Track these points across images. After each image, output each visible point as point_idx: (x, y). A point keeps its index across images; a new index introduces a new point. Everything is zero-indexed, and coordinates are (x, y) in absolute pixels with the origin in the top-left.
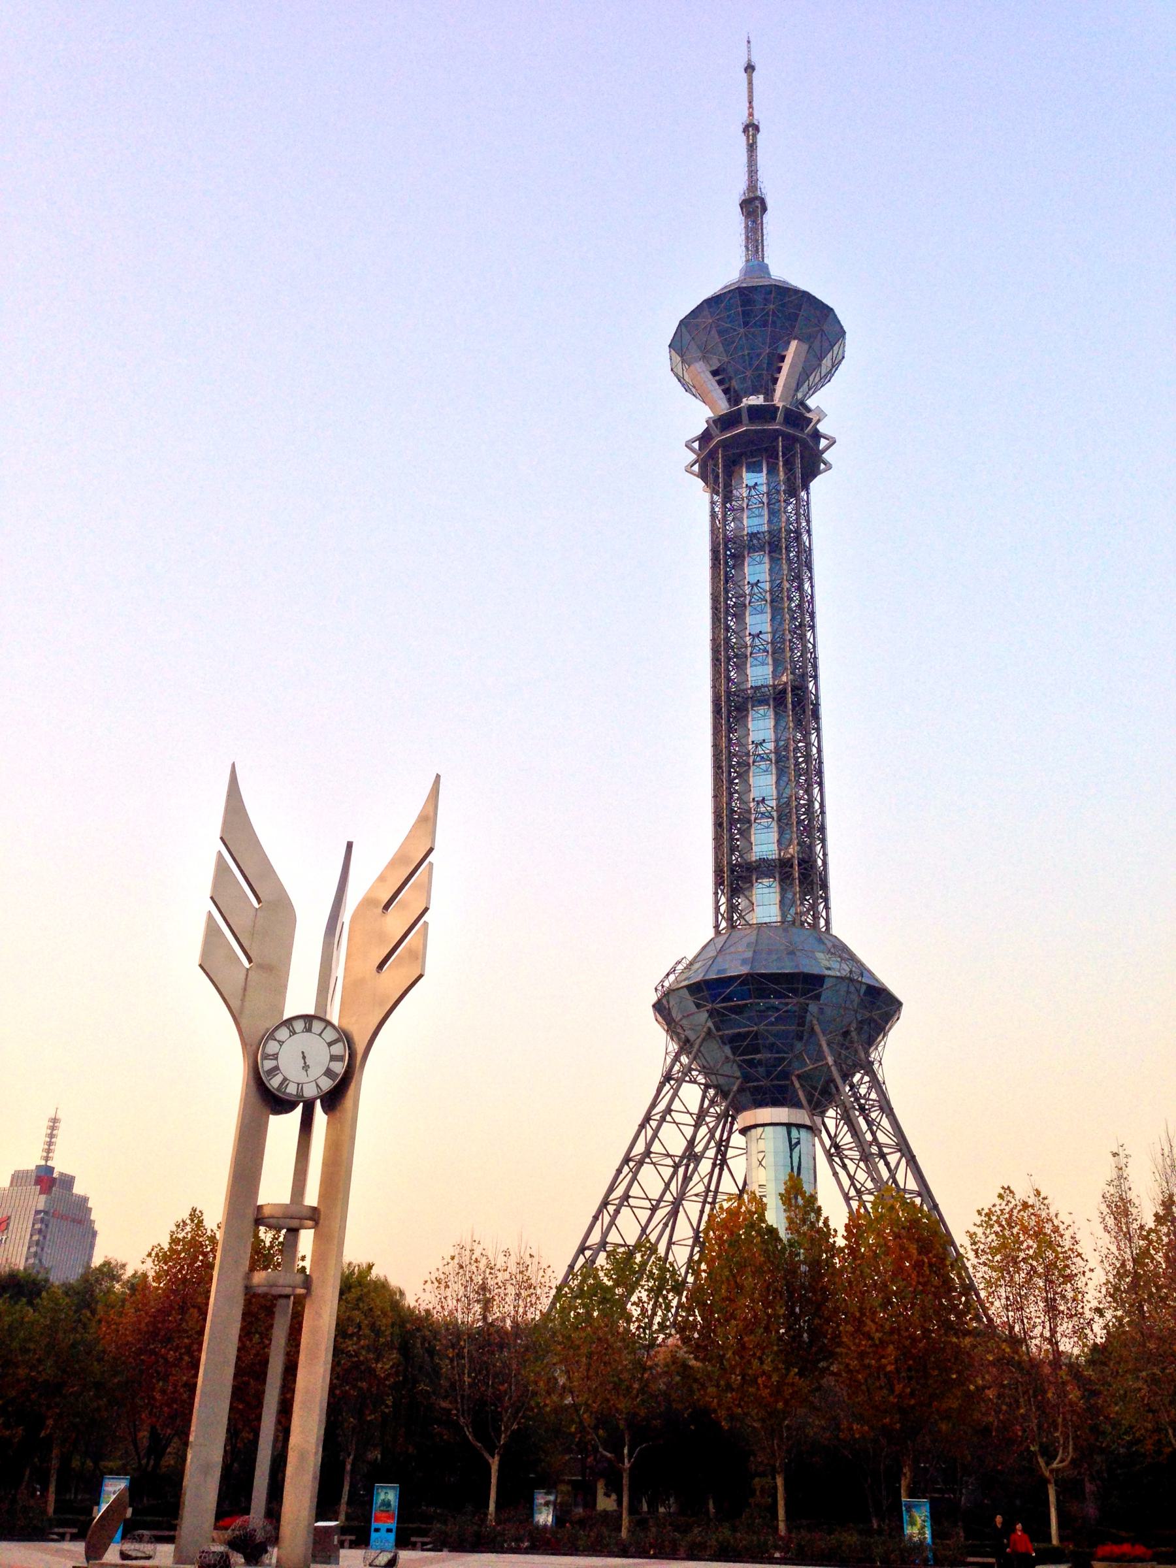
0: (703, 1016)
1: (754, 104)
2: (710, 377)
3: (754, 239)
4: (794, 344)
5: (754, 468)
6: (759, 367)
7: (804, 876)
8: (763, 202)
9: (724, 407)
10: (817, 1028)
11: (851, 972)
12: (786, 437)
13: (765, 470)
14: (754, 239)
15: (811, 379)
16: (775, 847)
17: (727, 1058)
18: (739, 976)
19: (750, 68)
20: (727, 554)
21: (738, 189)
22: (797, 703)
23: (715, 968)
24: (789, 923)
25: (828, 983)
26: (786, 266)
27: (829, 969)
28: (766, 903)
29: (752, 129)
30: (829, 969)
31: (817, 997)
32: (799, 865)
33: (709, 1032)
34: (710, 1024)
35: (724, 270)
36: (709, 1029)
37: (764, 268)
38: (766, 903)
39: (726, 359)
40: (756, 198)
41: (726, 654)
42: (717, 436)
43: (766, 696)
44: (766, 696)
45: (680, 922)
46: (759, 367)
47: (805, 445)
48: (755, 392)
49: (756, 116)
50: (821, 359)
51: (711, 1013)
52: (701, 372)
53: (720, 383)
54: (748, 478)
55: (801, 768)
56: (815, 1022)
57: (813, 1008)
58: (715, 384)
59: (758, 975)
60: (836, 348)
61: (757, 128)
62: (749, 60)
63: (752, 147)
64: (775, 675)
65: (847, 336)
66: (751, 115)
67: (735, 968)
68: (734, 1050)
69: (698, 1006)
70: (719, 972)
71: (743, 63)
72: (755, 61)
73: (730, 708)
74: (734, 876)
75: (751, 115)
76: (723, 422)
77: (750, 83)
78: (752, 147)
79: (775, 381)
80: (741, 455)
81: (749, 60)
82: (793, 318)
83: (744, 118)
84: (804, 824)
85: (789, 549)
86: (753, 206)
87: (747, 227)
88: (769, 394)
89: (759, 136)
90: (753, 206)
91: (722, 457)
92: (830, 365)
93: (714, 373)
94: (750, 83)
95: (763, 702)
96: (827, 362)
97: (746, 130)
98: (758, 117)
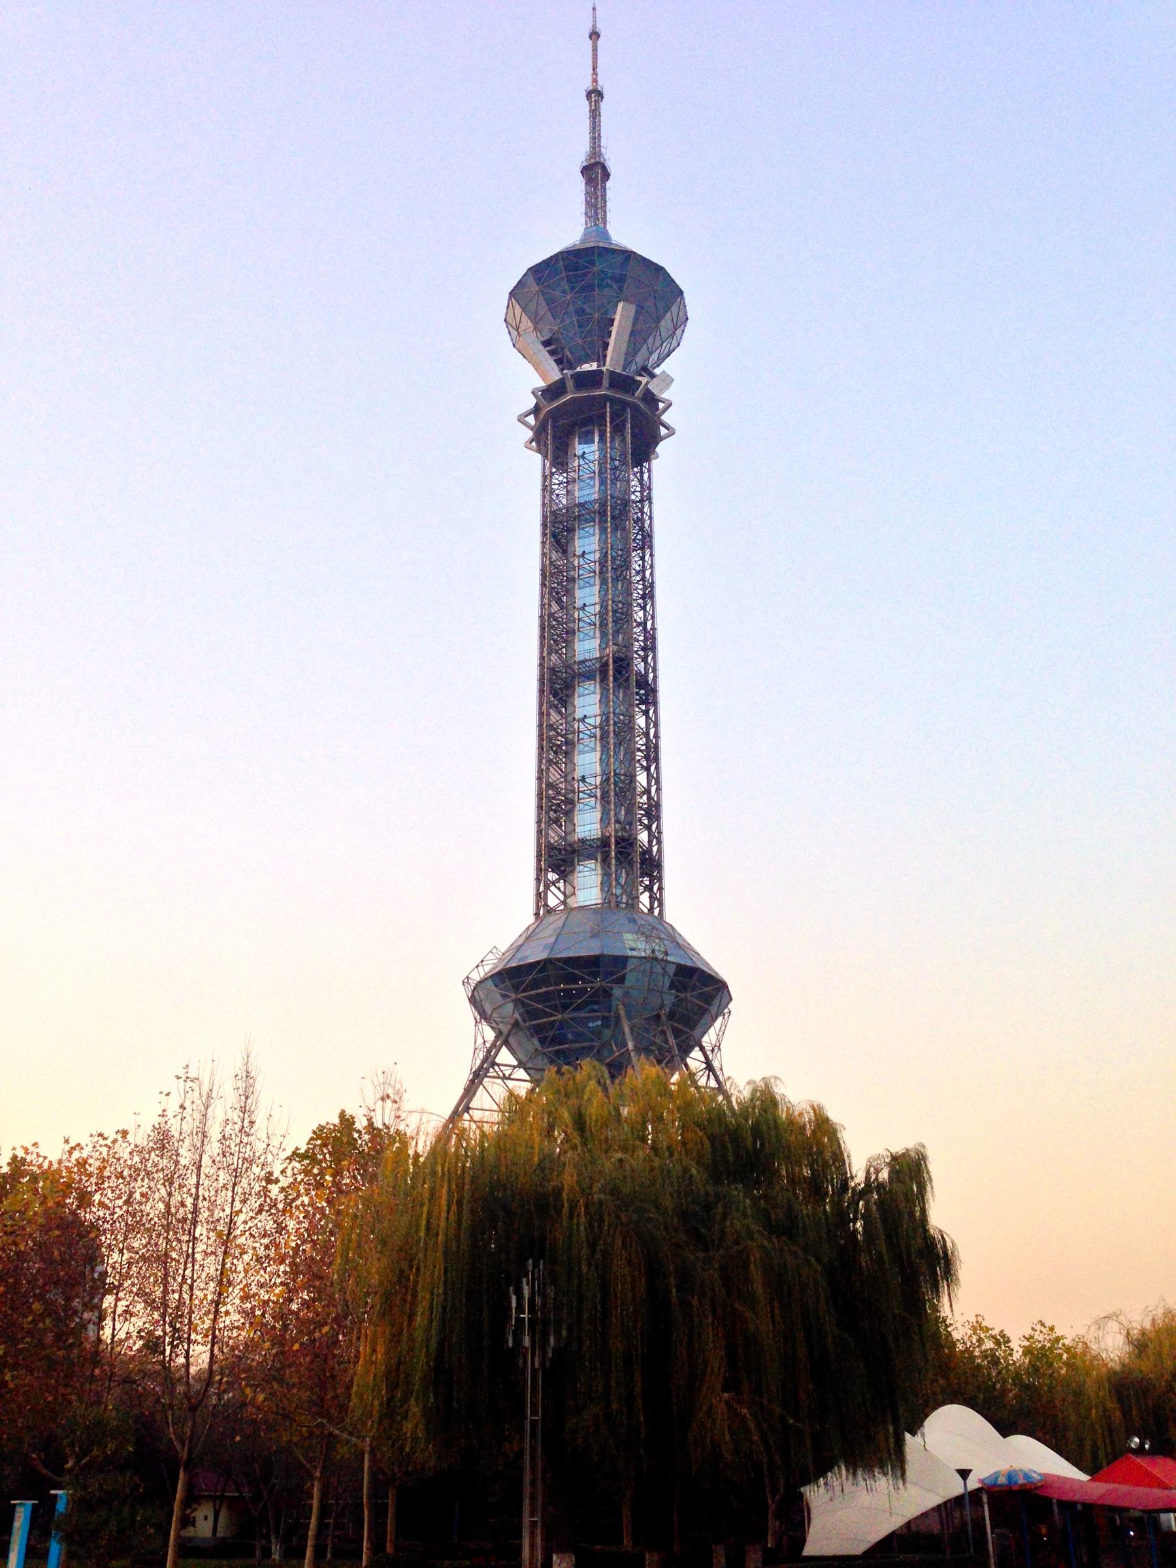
0: (510, 1007)
1: (599, 70)
2: (541, 347)
3: (596, 205)
4: (621, 305)
5: (587, 439)
6: (598, 346)
7: (633, 858)
8: (604, 168)
9: (555, 375)
10: (622, 1013)
11: (653, 951)
12: (613, 401)
13: (597, 439)
14: (596, 205)
15: (650, 341)
16: (598, 826)
17: (536, 1050)
18: (538, 962)
19: (595, 35)
20: (558, 530)
21: (580, 154)
22: (629, 678)
23: (519, 955)
24: (610, 903)
25: (631, 965)
26: (627, 231)
27: (632, 949)
28: (589, 885)
29: (595, 95)
30: (632, 949)
31: (621, 980)
32: (617, 843)
33: (516, 1024)
34: (517, 1015)
35: (566, 231)
36: (517, 1020)
37: (605, 234)
38: (589, 885)
39: (556, 328)
40: (597, 164)
41: (555, 630)
42: (545, 407)
43: (598, 674)
44: (598, 674)
45: (500, 908)
46: (598, 346)
47: (635, 408)
48: (588, 360)
49: (600, 83)
50: (659, 320)
51: (517, 1002)
52: (534, 341)
53: (552, 353)
54: (579, 449)
55: (631, 747)
56: (621, 1007)
57: (617, 992)
58: (547, 355)
59: (559, 960)
60: (674, 309)
61: (600, 95)
62: (594, 26)
63: (595, 114)
64: (601, 649)
65: (686, 295)
66: (595, 81)
67: (536, 954)
68: (542, 1041)
69: (504, 996)
70: (521, 959)
71: (588, 29)
72: (600, 27)
73: (557, 687)
74: (557, 859)
75: (595, 81)
76: (552, 392)
77: (595, 50)
78: (595, 114)
79: (606, 345)
80: (574, 425)
81: (594, 26)
82: (621, 280)
83: (588, 84)
84: (632, 803)
85: (624, 523)
86: (595, 173)
87: (587, 193)
88: (601, 359)
89: (603, 105)
90: (595, 173)
91: (558, 426)
92: (670, 326)
93: (546, 344)
94: (595, 50)
95: (588, 676)
96: (665, 324)
97: (586, 170)
98: (604, 83)
